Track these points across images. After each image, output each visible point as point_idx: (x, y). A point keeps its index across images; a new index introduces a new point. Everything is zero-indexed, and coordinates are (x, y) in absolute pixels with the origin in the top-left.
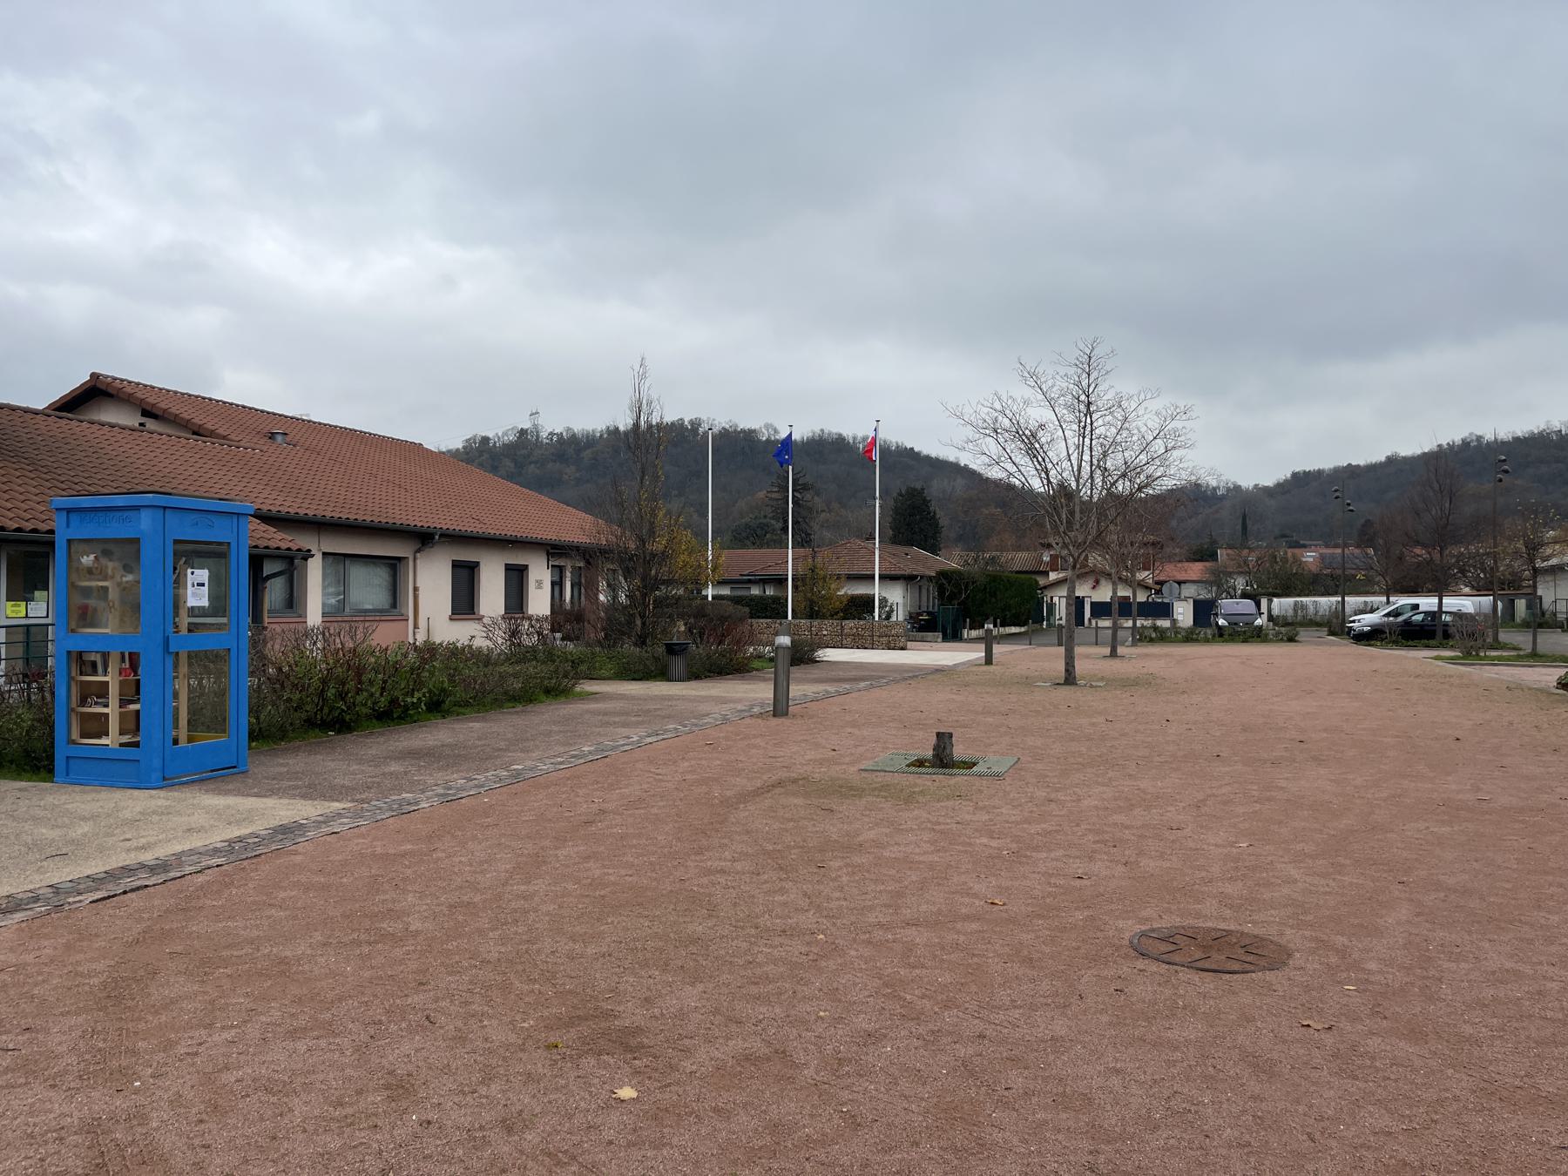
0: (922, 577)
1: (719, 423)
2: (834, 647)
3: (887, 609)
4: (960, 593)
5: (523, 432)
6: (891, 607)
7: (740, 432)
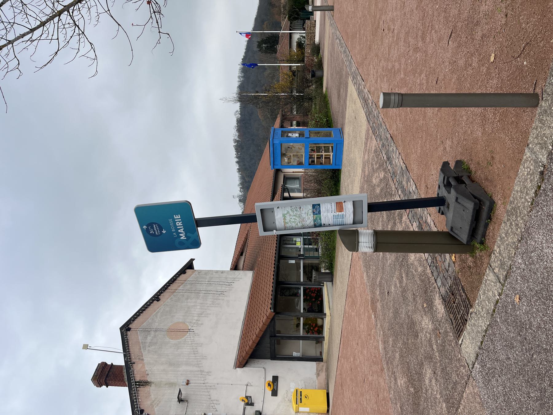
0: (290, 27)
1: (235, 132)
2: (315, 25)
3: (301, 38)
4: (296, 11)
5: (240, 201)
6: (301, 36)
7: (238, 125)
